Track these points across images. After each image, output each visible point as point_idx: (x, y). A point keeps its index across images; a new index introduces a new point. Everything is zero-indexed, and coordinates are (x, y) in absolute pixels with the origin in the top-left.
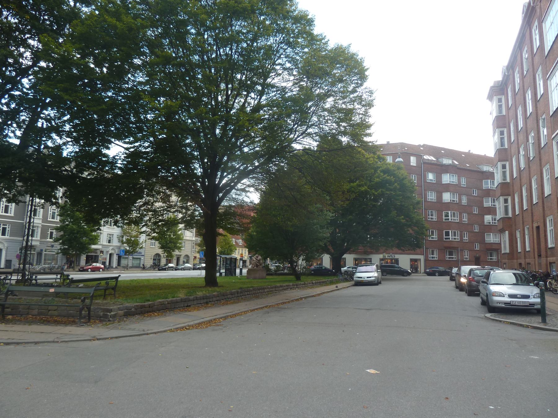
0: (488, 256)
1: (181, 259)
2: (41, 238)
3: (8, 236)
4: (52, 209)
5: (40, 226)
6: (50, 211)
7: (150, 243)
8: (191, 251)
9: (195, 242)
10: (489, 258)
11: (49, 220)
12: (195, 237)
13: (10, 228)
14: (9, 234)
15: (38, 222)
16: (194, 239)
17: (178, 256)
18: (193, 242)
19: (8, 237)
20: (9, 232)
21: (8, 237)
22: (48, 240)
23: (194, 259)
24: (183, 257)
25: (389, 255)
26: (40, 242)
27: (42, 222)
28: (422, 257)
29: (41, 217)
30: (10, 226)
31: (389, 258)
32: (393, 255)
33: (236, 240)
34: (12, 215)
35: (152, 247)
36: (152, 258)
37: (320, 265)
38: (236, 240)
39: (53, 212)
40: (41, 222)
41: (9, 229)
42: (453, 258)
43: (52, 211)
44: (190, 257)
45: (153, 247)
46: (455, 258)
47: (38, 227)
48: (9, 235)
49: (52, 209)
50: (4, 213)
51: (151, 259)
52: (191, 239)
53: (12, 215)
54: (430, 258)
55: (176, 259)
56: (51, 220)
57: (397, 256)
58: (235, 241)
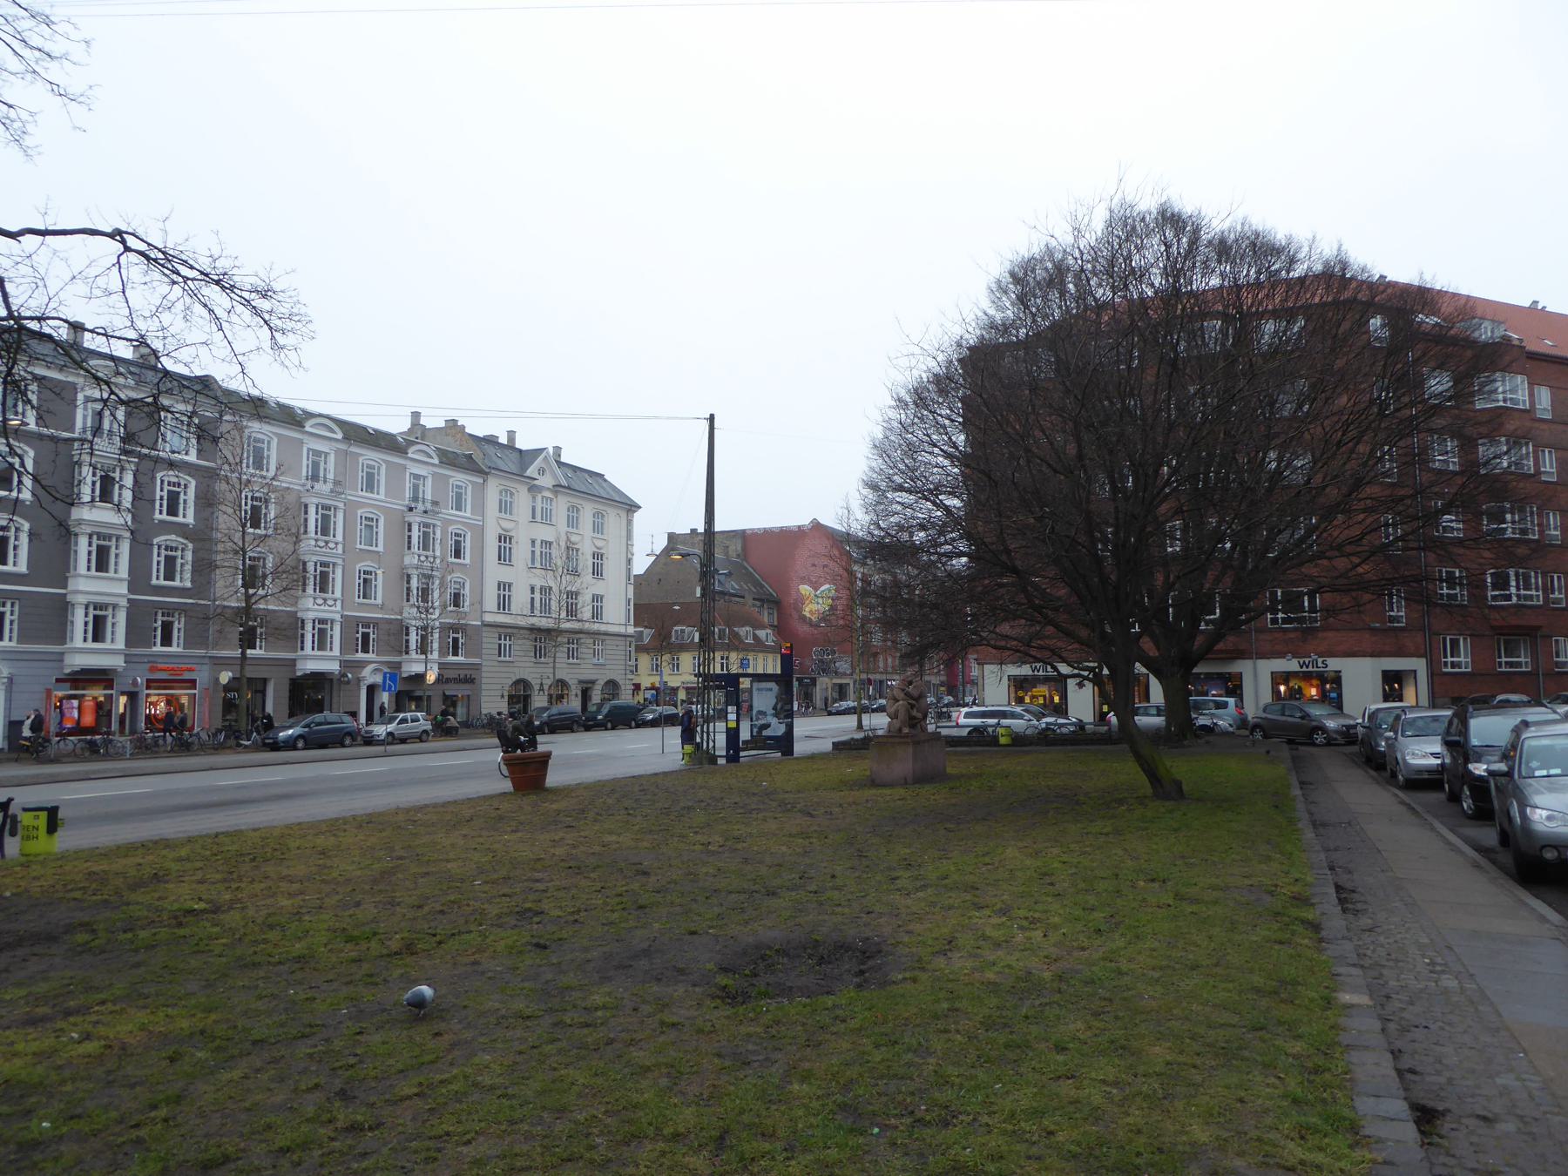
0: (1499, 651)
1: (595, 692)
2: (128, 643)
3: (10, 640)
4: (166, 483)
5: (124, 602)
6: (158, 488)
7: (592, 651)
8: (623, 667)
9: (633, 640)
10: (1504, 659)
11: (154, 581)
12: (636, 625)
13: (16, 613)
14: (182, 641)
15: (108, 591)
16: (631, 630)
17: (585, 685)
18: (629, 639)
19: (12, 644)
20: (15, 626)
21: (12, 644)
22: (154, 649)
23: (634, 691)
24: (600, 687)
25: (1307, 660)
26: (126, 655)
27: (130, 590)
28: (1419, 665)
29: (124, 572)
30: (16, 608)
31: (1304, 669)
32: (1320, 660)
33: (757, 632)
34: (22, 568)
35: (502, 658)
36: (506, 694)
37: (869, 682)
38: (757, 632)
39: (166, 556)
40: (126, 592)
41: (15, 617)
42: (1519, 664)
43: (166, 487)
44: (623, 687)
45: (507, 658)
46: (1526, 663)
47: (115, 607)
48: (15, 638)
49: (166, 483)
50: (162, 645)
51: (503, 696)
52: (622, 630)
53: (22, 568)
54: (1500, 666)
55: (579, 693)
56: (162, 582)
57: (1334, 664)
58: (754, 635)
